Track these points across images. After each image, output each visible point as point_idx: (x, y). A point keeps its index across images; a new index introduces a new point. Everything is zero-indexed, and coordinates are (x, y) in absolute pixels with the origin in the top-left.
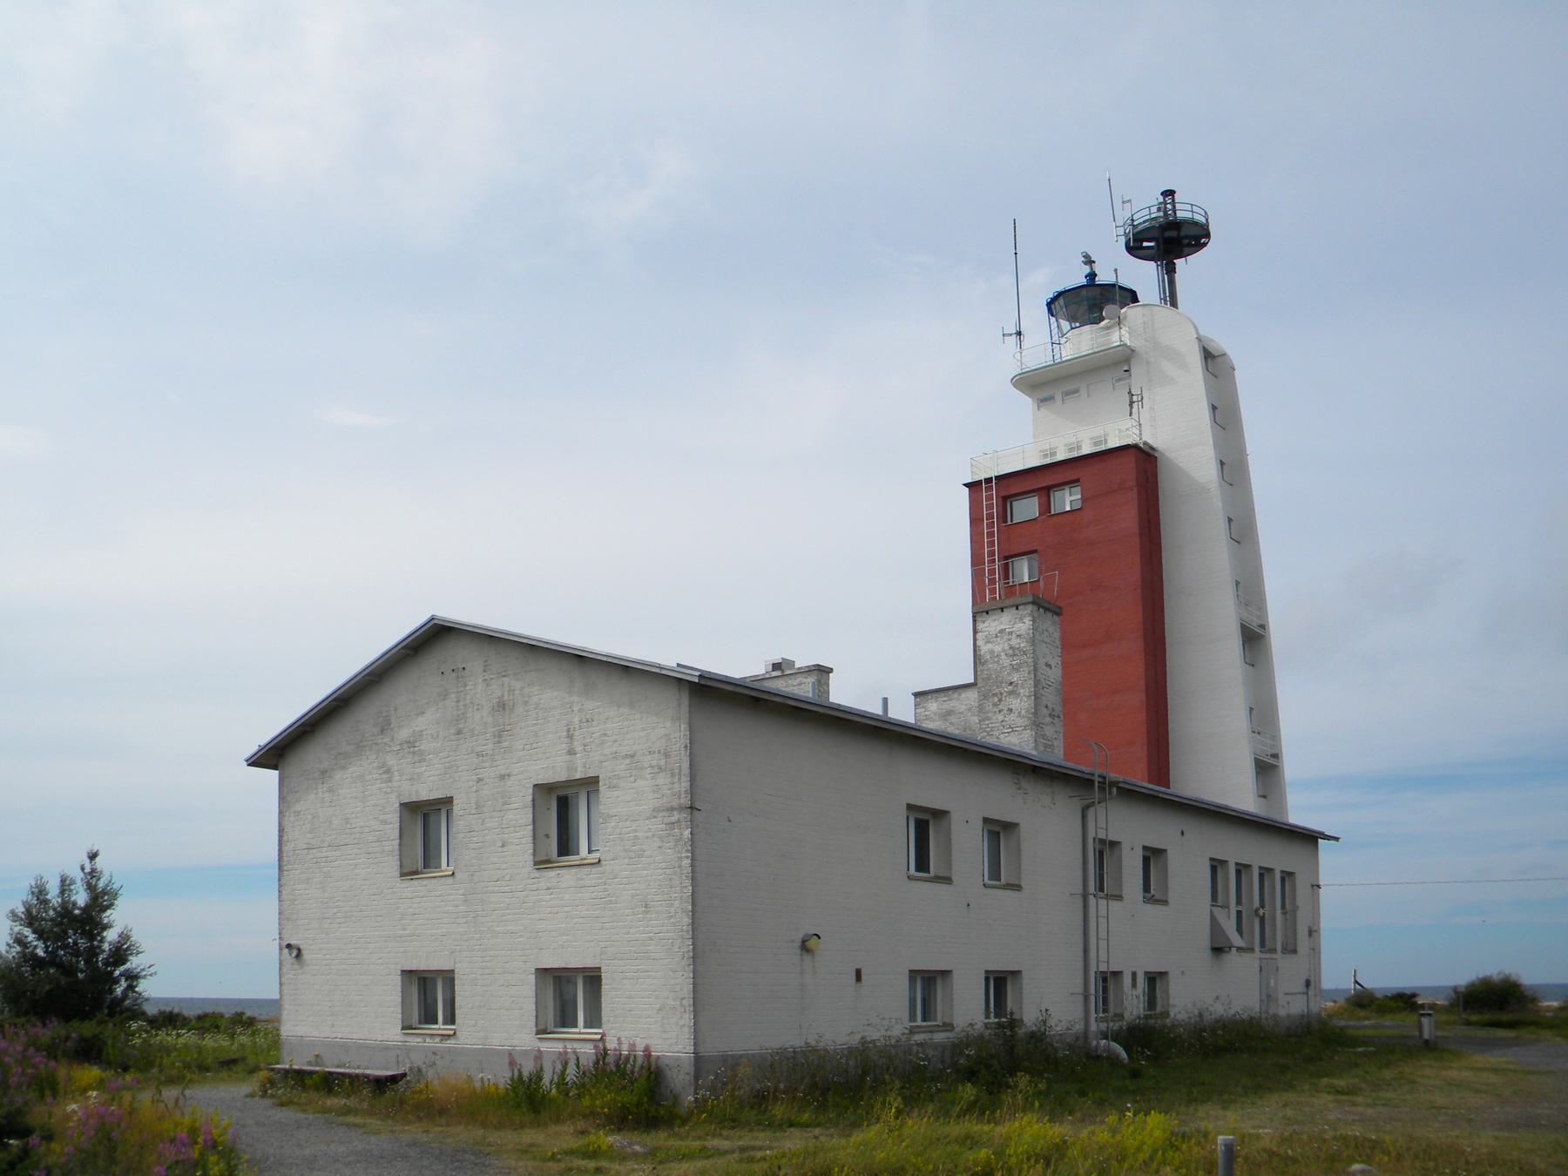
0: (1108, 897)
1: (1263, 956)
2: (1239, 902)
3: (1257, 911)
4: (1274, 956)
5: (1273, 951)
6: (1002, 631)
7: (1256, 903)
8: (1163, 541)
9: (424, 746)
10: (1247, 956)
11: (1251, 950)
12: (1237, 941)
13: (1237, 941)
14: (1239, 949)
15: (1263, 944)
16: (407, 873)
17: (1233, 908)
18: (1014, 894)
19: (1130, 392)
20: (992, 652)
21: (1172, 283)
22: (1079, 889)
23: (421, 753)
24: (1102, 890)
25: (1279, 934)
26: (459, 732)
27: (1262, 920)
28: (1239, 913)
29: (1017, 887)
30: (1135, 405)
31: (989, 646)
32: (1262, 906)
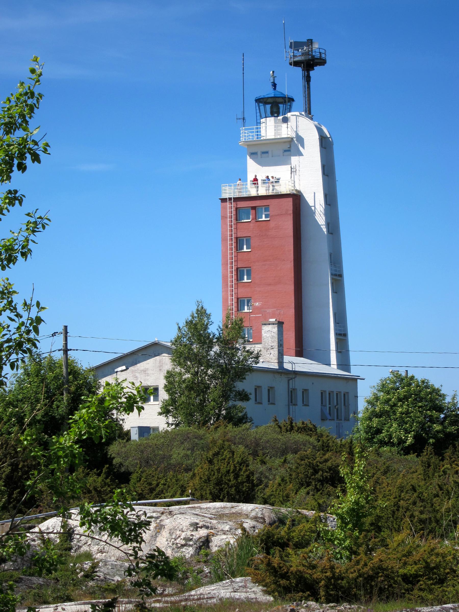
0: (294, 405)
1: (338, 422)
2: (330, 404)
3: (335, 406)
4: (341, 422)
5: (341, 420)
6: (269, 330)
7: (335, 404)
8: (302, 236)
9: (149, 372)
10: (332, 422)
11: (334, 420)
12: (329, 417)
13: (329, 417)
14: (330, 420)
15: (337, 418)
16: (348, 393)
17: (328, 406)
18: (260, 405)
19: (291, 167)
20: (266, 336)
21: (309, 88)
22: (287, 404)
23: (148, 374)
24: (291, 402)
25: (343, 414)
26: (160, 370)
27: (337, 410)
28: (330, 407)
29: (274, 404)
30: (293, 173)
31: (266, 334)
32: (337, 404)
